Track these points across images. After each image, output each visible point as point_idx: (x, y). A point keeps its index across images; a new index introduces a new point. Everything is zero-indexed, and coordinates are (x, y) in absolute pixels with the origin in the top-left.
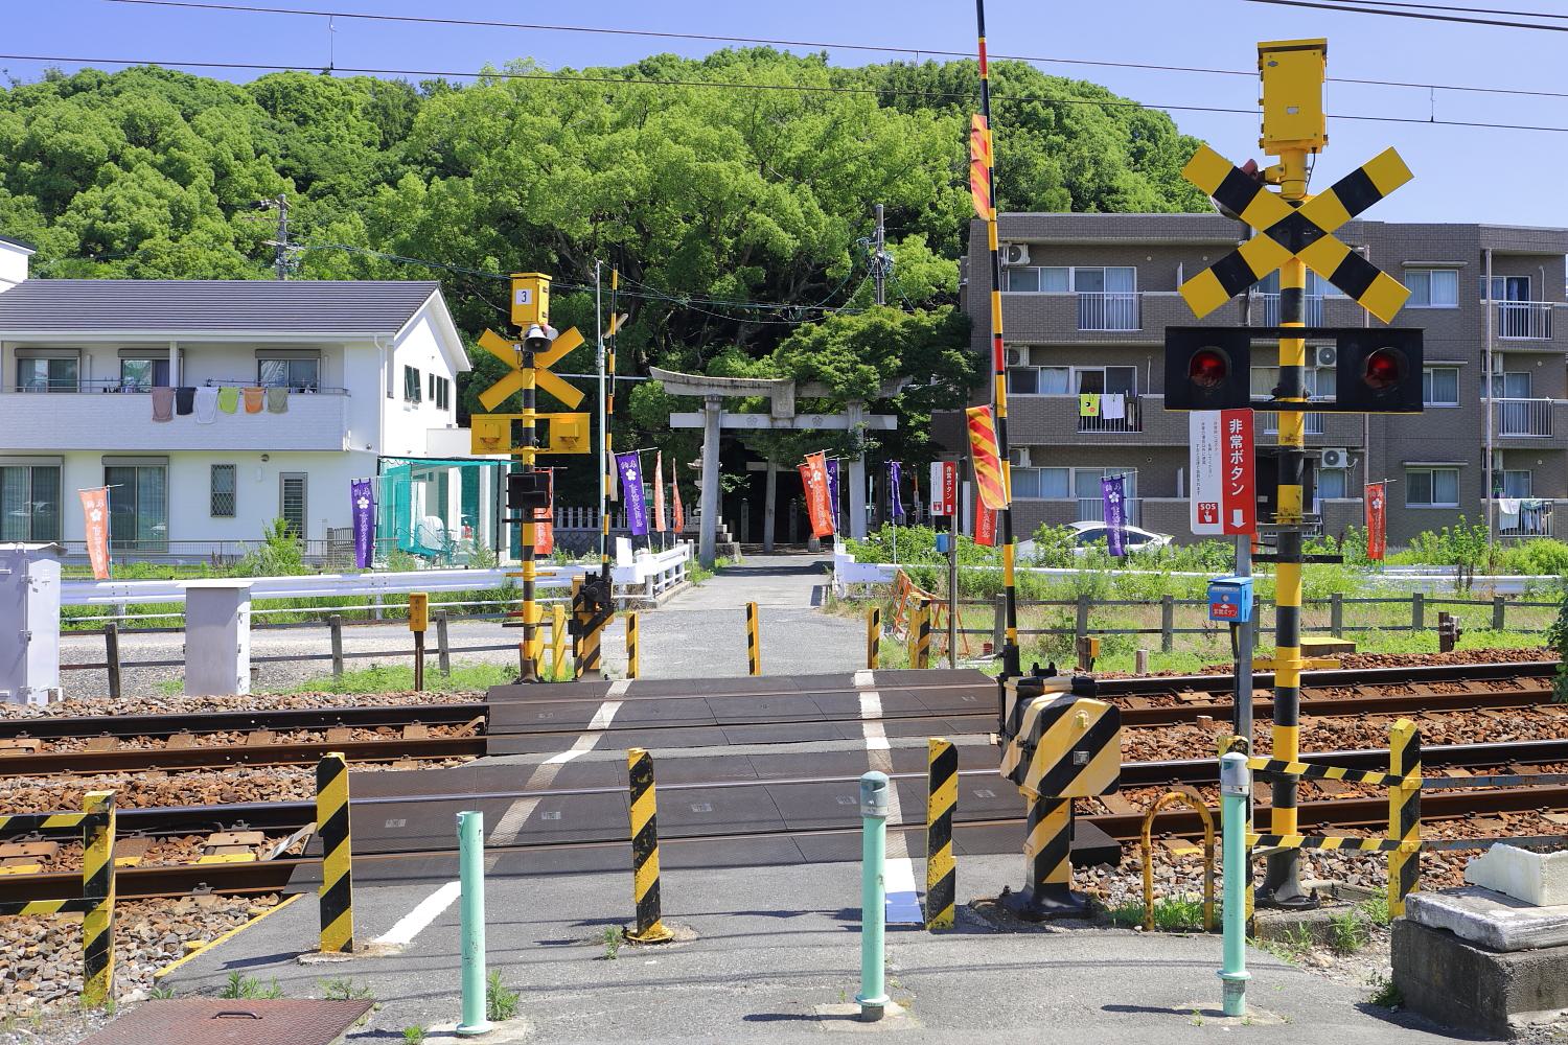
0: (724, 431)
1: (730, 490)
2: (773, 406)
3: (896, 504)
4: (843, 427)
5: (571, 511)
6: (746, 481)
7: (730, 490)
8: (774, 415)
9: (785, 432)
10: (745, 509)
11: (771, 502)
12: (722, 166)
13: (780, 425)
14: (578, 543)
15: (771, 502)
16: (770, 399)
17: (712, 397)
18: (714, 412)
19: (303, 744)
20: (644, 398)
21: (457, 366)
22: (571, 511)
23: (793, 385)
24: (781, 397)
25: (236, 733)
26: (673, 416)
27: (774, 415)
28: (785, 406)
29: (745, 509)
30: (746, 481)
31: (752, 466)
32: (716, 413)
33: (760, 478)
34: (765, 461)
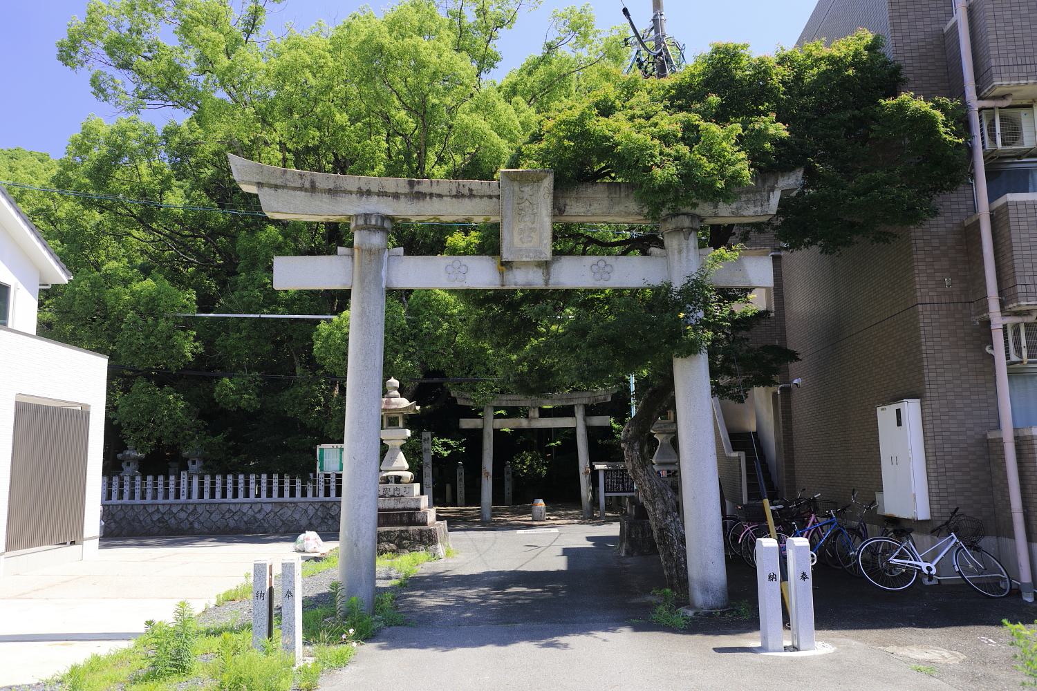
0: (398, 295)
1: (446, 454)
2: (505, 234)
3: (333, 479)
4: (656, 281)
5: (219, 479)
6: (461, 445)
7: (446, 454)
8: (506, 256)
9: (535, 296)
10: (461, 472)
11: (488, 464)
12: (423, 43)
13: (523, 279)
14: (260, 516)
15: (488, 464)
16: (496, 226)
17: (367, 216)
18: (370, 251)
19: (429, 490)
20: (330, 334)
21: (41, 274)
22: (219, 479)
23: (548, 182)
24: (520, 212)
25: (609, 399)
26: (279, 262)
27: (506, 256)
28: (528, 234)
29: (461, 472)
30: (461, 445)
31: (466, 423)
32: (374, 254)
33: (475, 437)
34: (480, 417)
